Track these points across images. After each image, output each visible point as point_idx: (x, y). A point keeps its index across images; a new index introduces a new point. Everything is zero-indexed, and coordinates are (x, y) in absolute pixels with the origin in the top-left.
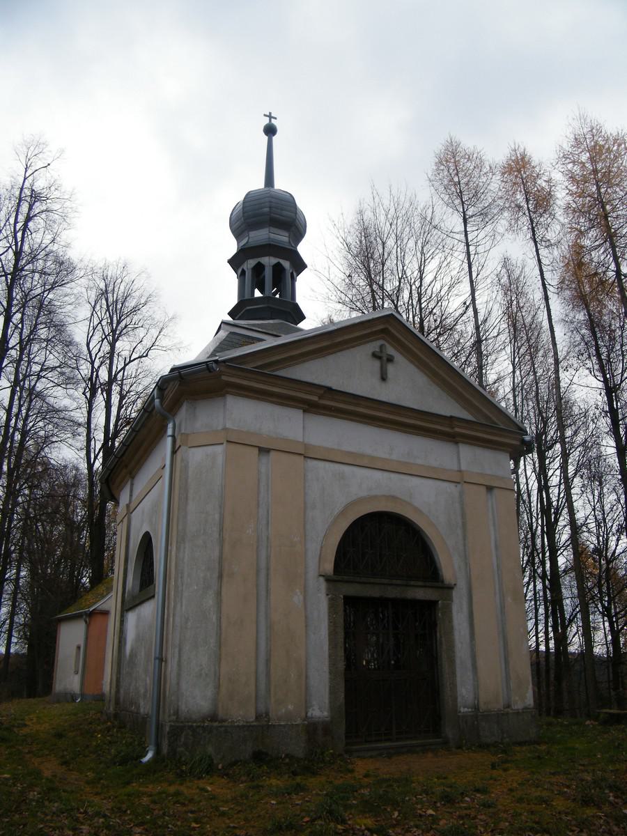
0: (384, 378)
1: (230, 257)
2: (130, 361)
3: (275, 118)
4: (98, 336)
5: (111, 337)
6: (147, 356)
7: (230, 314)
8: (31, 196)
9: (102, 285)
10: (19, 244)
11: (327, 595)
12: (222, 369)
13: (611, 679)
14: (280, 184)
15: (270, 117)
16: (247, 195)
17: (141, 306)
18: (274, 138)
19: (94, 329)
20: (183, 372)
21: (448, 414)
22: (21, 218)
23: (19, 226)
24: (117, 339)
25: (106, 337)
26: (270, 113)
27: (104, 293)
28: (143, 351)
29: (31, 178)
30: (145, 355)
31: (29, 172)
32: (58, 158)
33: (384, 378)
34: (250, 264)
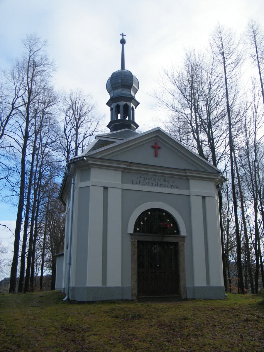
0: (156, 155)
1: (107, 102)
2: (85, 138)
3: (125, 35)
4: (69, 127)
5: (76, 127)
6: (92, 135)
7: (108, 126)
8: (34, 65)
9: (70, 103)
10: (30, 89)
11: (131, 240)
12: (88, 159)
13: (30, 232)
14: (128, 67)
15: (123, 35)
16: (113, 73)
17: (89, 111)
18: (125, 45)
19: (67, 125)
20: (74, 161)
21: (183, 168)
22: (30, 75)
23: (29, 80)
24: (79, 128)
25: (73, 127)
26: (123, 33)
27: (72, 107)
28: (91, 133)
29: (33, 56)
30: (91, 134)
31: (32, 53)
32: (44, 45)
33: (156, 155)
34: (115, 105)
